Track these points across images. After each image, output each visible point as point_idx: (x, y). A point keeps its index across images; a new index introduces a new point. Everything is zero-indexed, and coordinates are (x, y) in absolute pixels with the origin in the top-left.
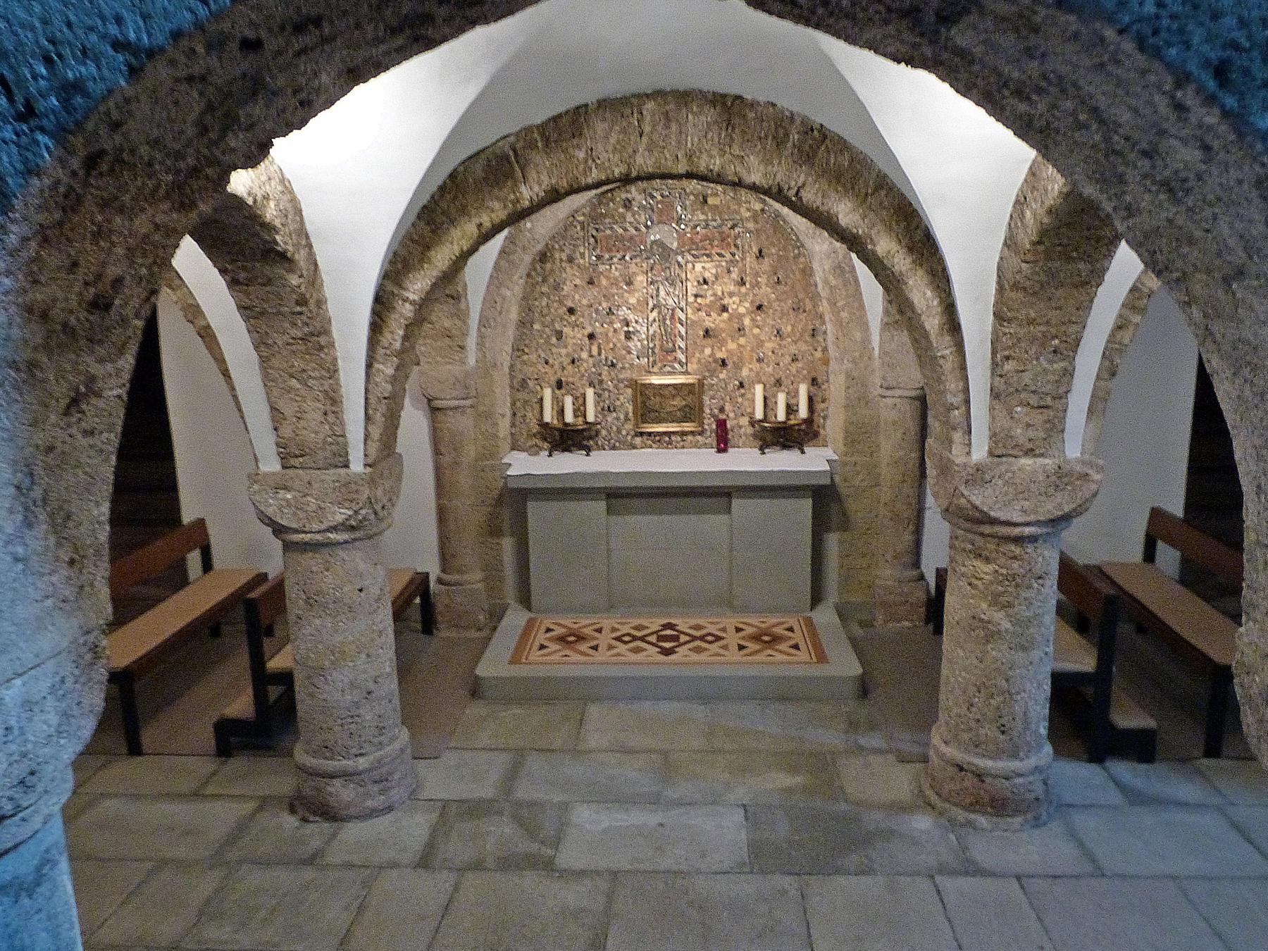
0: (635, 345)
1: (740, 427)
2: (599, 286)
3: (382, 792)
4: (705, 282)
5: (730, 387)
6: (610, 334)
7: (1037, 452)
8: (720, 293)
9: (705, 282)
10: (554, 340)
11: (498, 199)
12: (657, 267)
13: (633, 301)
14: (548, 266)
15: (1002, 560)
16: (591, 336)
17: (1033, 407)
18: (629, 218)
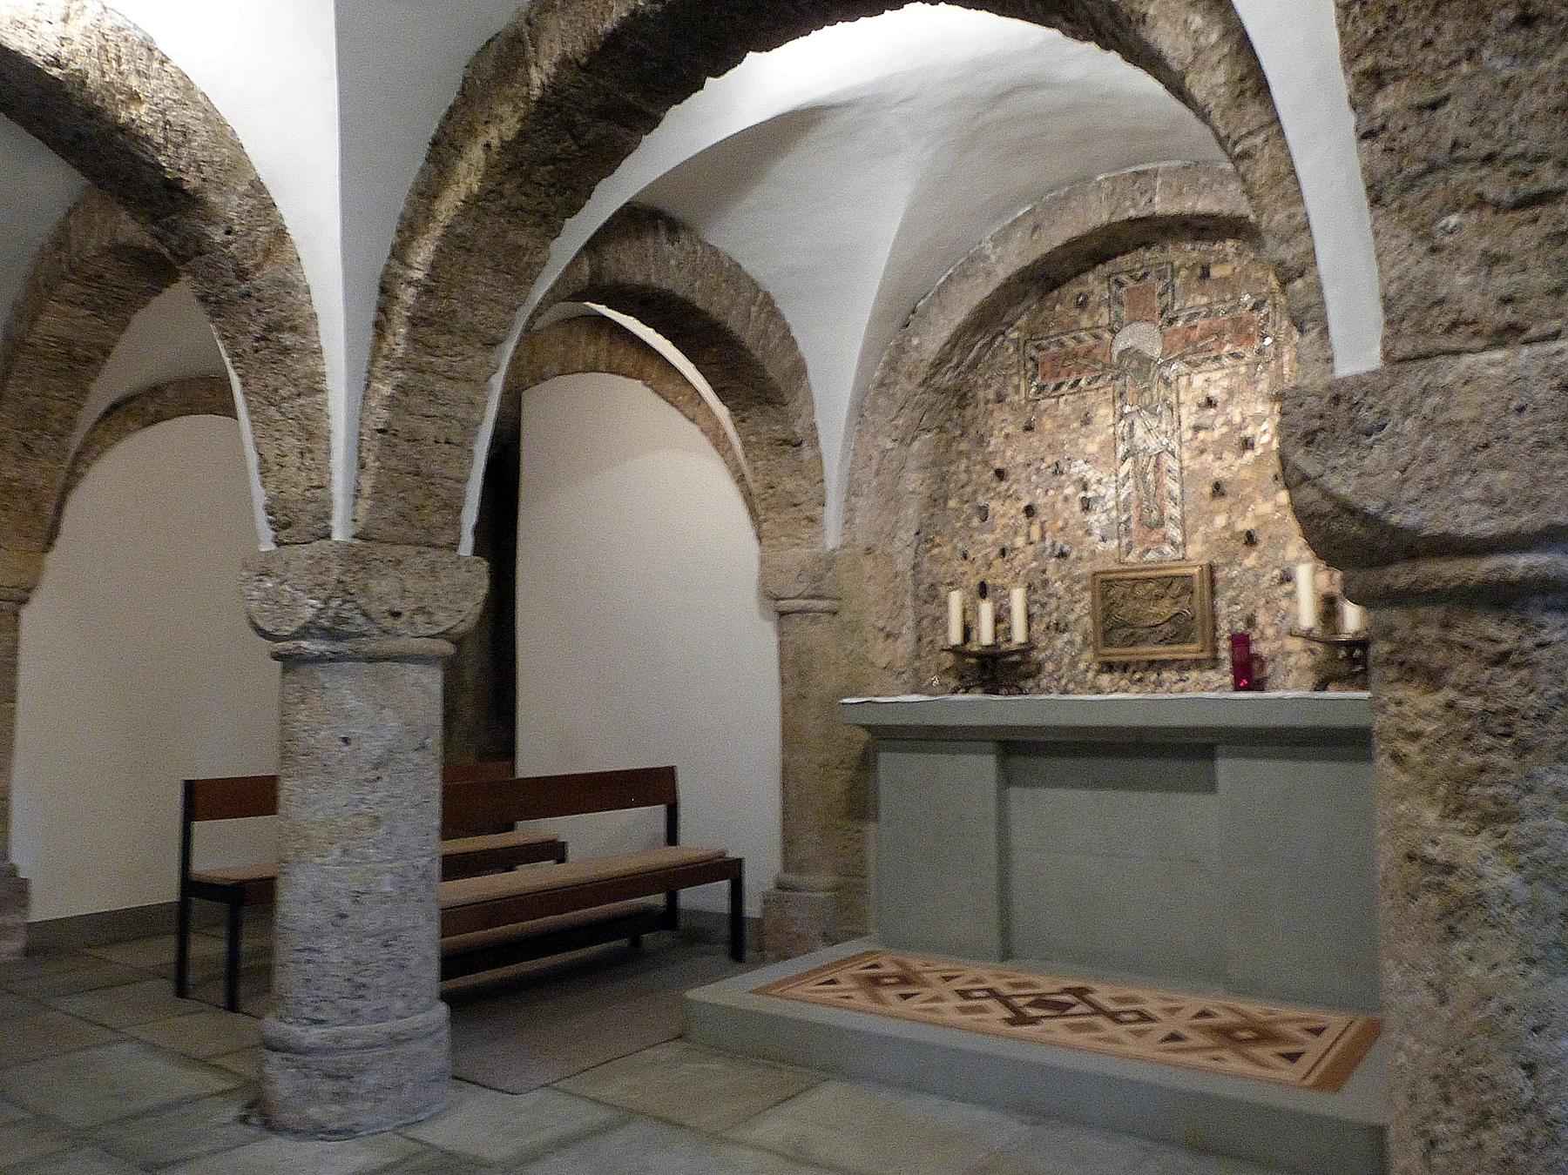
0: (1097, 519)
1: (1289, 654)
2: (1041, 433)
3: (338, 1097)
4: (1210, 403)
5: (1265, 582)
6: (1059, 505)
7: (1534, 331)
8: (1237, 419)
9: (1210, 403)
10: (976, 522)
11: (507, 99)
12: (1130, 391)
13: (1092, 448)
14: (969, 412)
15: (1464, 670)
16: (1030, 511)
17: (1498, 207)
18: (1085, 322)
